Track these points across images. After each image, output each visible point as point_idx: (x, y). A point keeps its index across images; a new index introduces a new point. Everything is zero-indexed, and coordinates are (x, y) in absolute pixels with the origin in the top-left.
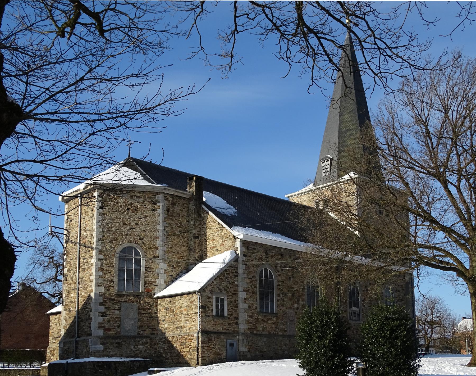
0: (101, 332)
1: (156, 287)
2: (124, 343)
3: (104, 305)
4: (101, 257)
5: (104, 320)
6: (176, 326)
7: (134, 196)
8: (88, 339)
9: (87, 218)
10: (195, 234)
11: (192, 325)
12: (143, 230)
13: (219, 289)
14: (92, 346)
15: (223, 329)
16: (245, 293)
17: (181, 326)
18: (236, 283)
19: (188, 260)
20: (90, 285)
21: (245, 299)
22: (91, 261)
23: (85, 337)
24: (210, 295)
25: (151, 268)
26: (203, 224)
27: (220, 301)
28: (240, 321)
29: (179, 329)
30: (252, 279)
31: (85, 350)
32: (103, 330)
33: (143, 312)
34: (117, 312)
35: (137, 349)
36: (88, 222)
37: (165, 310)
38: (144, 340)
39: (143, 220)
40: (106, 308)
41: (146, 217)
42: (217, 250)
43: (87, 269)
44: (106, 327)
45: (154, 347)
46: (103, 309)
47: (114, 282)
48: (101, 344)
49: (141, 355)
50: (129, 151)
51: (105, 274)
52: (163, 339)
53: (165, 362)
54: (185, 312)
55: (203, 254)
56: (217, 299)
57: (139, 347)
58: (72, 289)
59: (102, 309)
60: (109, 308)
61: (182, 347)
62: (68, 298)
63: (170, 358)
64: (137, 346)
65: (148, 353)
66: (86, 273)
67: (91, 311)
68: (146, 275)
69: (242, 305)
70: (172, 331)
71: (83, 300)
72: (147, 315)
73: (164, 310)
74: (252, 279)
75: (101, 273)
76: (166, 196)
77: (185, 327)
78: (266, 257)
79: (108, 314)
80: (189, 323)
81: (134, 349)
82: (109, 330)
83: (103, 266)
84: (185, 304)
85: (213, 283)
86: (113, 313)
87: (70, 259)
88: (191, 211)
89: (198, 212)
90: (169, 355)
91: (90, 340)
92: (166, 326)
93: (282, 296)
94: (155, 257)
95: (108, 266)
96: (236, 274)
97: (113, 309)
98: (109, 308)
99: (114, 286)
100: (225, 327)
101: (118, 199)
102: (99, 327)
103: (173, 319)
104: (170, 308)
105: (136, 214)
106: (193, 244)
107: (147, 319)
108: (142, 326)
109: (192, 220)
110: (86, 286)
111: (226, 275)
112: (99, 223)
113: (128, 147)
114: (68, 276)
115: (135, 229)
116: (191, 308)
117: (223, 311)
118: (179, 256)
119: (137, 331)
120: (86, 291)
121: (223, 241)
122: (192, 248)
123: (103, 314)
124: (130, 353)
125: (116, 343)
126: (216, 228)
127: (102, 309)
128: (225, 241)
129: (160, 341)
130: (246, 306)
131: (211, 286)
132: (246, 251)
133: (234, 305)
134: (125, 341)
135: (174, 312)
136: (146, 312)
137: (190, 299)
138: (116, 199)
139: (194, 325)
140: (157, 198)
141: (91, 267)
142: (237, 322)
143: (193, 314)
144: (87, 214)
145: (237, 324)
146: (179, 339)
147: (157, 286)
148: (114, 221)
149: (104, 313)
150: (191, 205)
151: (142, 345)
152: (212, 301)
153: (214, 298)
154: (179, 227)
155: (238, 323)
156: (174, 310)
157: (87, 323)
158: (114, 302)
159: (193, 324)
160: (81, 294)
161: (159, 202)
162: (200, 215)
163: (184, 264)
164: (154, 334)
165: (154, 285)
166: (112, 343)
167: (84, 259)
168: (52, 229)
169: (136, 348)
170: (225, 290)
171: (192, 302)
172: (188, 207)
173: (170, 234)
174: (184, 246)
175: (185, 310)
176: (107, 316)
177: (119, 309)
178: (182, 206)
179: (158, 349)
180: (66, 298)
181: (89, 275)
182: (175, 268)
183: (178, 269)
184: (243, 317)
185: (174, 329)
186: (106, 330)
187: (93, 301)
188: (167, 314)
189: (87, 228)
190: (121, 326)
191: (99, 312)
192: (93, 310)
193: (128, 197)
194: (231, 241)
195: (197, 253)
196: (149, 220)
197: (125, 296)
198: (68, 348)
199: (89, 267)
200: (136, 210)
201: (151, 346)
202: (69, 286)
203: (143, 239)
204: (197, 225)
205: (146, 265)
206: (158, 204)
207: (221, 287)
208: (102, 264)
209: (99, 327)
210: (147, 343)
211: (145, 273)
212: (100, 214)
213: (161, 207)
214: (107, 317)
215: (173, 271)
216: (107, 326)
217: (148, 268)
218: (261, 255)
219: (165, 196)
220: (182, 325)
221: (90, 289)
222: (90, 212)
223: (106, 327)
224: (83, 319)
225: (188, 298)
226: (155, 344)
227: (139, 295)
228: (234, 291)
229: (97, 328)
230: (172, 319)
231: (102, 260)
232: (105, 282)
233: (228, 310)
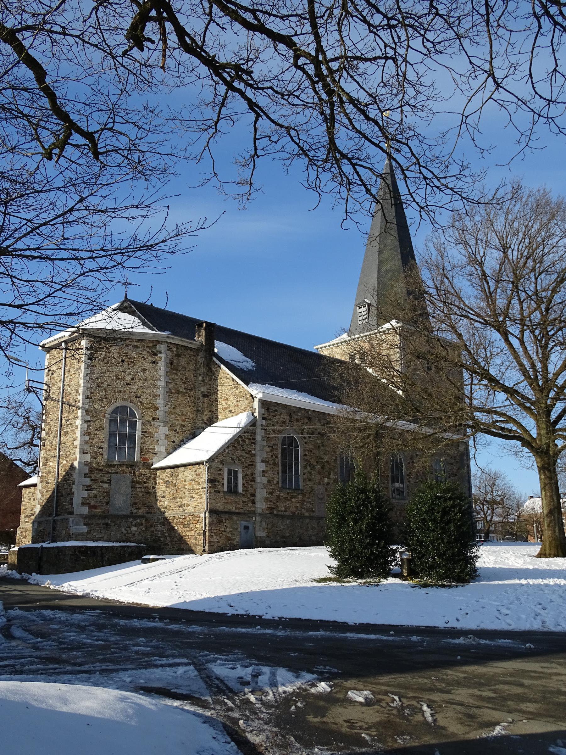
0: (85, 510)
2: (113, 524)
5: (89, 495)
6: (178, 504)
8: (67, 519)
9: (72, 371)
13: (233, 460)
18: (253, 452)
21: (263, 471)
23: (66, 516)
24: (220, 466)
27: (233, 474)
28: (257, 499)
33: (138, 485)
34: (105, 486)
38: (138, 521)
39: (140, 374)
40: (92, 480)
41: (144, 370)
47: (102, 448)
48: (85, 524)
54: (189, 487)
56: (230, 472)
59: (88, 481)
61: (185, 529)
67: (73, 484)
68: (143, 441)
69: (259, 479)
72: (143, 490)
77: (189, 505)
81: (125, 532)
82: (95, 507)
90: (169, 539)
91: (71, 519)
92: (166, 503)
93: (309, 468)
95: (97, 430)
96: (253, 442)
100: (238, 506)
102: (83, 504)
106: (201, 404)
108: (136, 504)
117: (236, 486)
120: (68, 459)
123: (89, 488)
130: (265, 480)
133: (250, 479)
140: (158, 348)
145: (253, 502)
147: (156, 454)
149: (90, 486)
151: (135, 526)
153: (226, 470)
154: (184, 383)
157: (68, 499)
159: (199, 501)
161: (161, 353)
164: (151, 513)
166: (98, 524)
167: (66, 420)
170: (240, 460)
171: (199, 475)
172: (196, 360)
175: (190, 484)
177: (109, 482)
182: (178, 433)
184: (261, 494)
186: (91, 507)
187: (77, 471)
194: (248, 401)
196: (147, 374)
199: (73, 431)
200: (132, 362)
202: (48, 453)
205: (142, 429)
206: (159, 355)
207: (234, 457)
208: (89, 426)
211: (142, 438)
213: (163, 359)
216: (93, 503)
220: (186, 502)
222: (77, 364)
225: (194, 469)
226: (151, 526)
231: (89, 421)
232: (92, 449)
233: (243, 484)
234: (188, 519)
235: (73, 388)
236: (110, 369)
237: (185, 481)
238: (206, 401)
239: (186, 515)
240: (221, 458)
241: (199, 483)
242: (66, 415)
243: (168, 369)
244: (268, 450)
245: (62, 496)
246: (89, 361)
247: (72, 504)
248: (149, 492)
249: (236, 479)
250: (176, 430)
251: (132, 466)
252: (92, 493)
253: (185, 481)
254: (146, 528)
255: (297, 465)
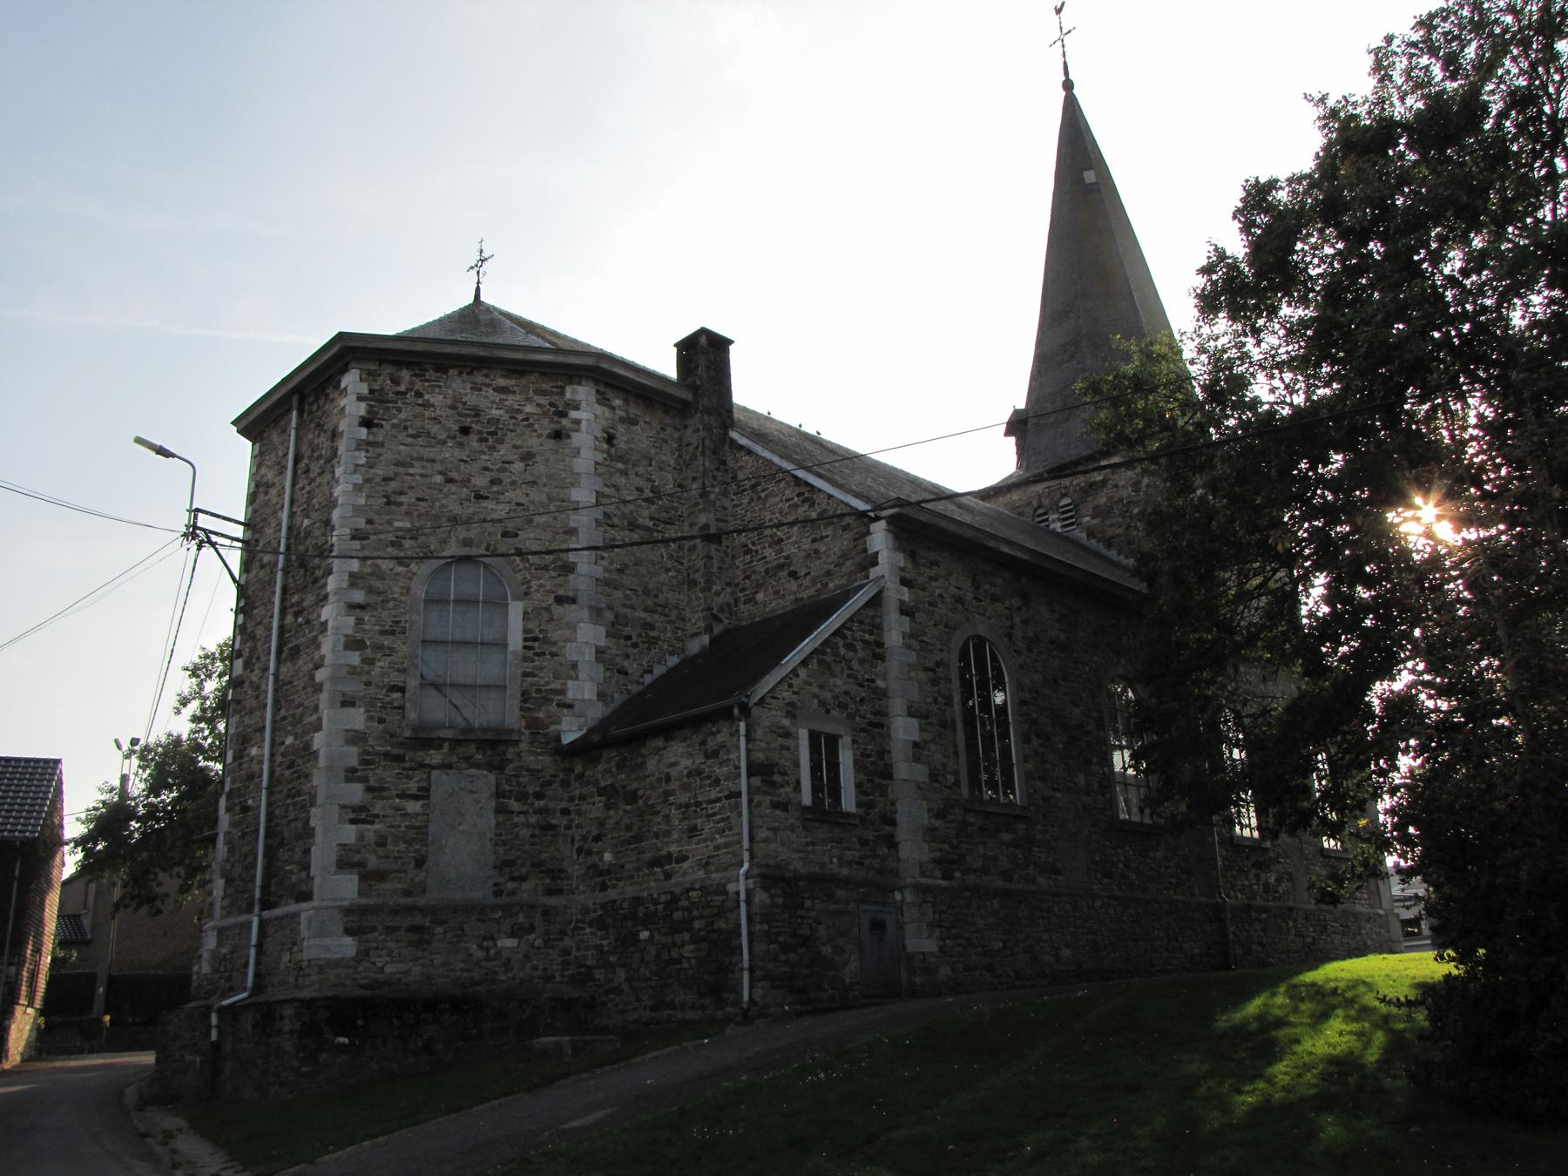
0: (348, 887)
1: (565, 711)
2: (439, 930)
3: (364, 780)
4: (359, 596)
5: (361, 837)
6: (648, 856)
7: (488, 385)
8: (296, 915)
9: (315, 469)
10: (706, 527)
11: (717, 848)
12: (518, 504)
13: (822, 703)
14: (312, 942)
15: (841, 865)
16: (915, 721)
17: (670, 855)
18: (880, 683)
19: (683, 620)
20: (312, 705)
21: (916, 745)
22: (319, 616)
23: (292, 907)
24: (786, 722)
25: (546, 641)
26: (735, 494)
27: (825, 747)
28: (903, 832)
29: (661, 866)
30: (934, 671)
31: (286, 957)
32: (356, 878)
33: (514, 805)
34: (413, 807)
35: (492, 951)
36: (318, 480)
37: (604, 798)
38: (521, 918)
39: (518, 466)
40: (369, 789)
41: (528, 457)
42: (794, 575)
43: (307, 647)
44: (370, 865)
45: (562, 944)
46: (360, 794)
47: (402, 690)
48: (349, 932)
49: (510, 975)
50: (478, 283)
51: (370, 662)
52: (595, 911)
53: (605, 1004)
54: (684, 798)
55: (736, 601)
56: (814, 737)
57: (499, 944)
58: (255, 731)
59: (355, 793)
60: (384, 789)
61: (678, 938)
62: (240, 765)
63: (625, 987)
64: (493, 939)
65: (535, 968)
66: (300, 662)
67: (313, 803)
68: (528, 667)
69: (904, 769)
70: (632, 877)
71: (286, 764)
72: (533, 819)
73: (597, 799)
74: (935, 673)
75: (355, 658)
76: (603, 389)
77: (685, 858)
78: (976, 599)
79: (377, 816)
80: (705, 840)
81: (480, 954)
82: (381, 876)
83: (365, 631)
84: (686, 763)
85: (797, 675)
86: (397, 809)
87: (253, 623)
88: (691, 448)
89: (715, 453)
90: (621, 973)
91: (303, 916)
92: (608, 857)
93: (1036, 742)
94: (560, 600)
95: (383, 633)
96: (877, 652)
97: (399, 796)
98: (384, 789)
99: (402, 708)
100: (849, 855)
101: (427, 397)
102: (344, 864)
103: (635, 828)
104: (624, 787)
105: (493, 448)
106: (700, 564)
107: (533, 836)
108: (511, 863)
109: (694, 479)
110: (300, 710)
111: (843, 651)
112: (357, 476)
113: (474, 272)
114: (247, 684)
115: (487, 498)
116: (709, 777)
117: (836, 792)
118: (650, 603)
119: (491, 882)
120: (299, 730)
121: (814, 540)
122: (697, 576)
123: (360, 815)
124: (462, 970)
125: (411, 929)
126: (787, 500)
127: (355, 793)
128: (822, 538)
129: (583, 921)
130: (921, 773)
131: (790, 686)
132: (910, 566)
133: (876, 771)
134: (445, 922)
135: (641, 802)
136: (525, 808)
137: (703, 743)
138: (419, 394)
139: (726, 845)
140: (568, 395)
141: (320, 636)
142: (891, 836)
143: (719, 800)
144: (316, 455)
145: (892, 843)
146: (660, 907)
147: (570, 706)
148: (411, 471)
149: (362, 808)
150: (690, 431)
151: (512, 935)
152: (797, 747)
153: (803, 735)
154: (648, 500)
155: (898, 839)
156: (640, 793)
157: (298, 852)
158: (404, 769)
159: (720, 840)
160: (283, 743)
161: (577, 408)
162: (724, 463)
163: (669, 634)
164: (559, 892)
165: (559, 705)
166: (391, 930)
167: (297, 615)
168: (196, 517)
169: (487, 950)
170: (843, 706)
171: (714, 754)
172: (680, 439)
173: (616, 521)
174: (668, 570)
175: (686, 787)
176: (372, 823)
177: (423, 794)
178: (658, 433)
179: (574, 953)
180: (236, 763)
181: (311, 666)
182: (635, 645)
183: (649, 649)
184: (911, 814)
185: (638, 869)
186: (369, 877)
187: (322, 762)
188: (612, 813)
189: (314, 501)
190: (429, 864)
191: (342, 807)
192: (320, 800)
193: (464, 389)
194: (848, 535)
195: (718, 594)
196: (539, 469)
197: (446, 745)
198: (232, 953)
199: (314, 640)
200: (494, 434)
201: (546, 942)
202: (247, 721)
203: (516, 535)
204: (712, 496)
205: (526, 631)
206: (573, 414)
207: (827, 695)
208: (360, 621)
209: (344, 864)
210: (532, 929)
211: (525, 659)
212: (358, 444)
213: (584, 425)
214: (377, 826)
215: (627, 656)
216: (373, 862)
217: (535, 639)
218: (960, 589)
219: (598, 391)
220: (674, 848)
221: (314, 717)
222: (327, 444)
223: (370, 865)
224: (286, 834)
225: (696, 739)
226: (563, 933)
227: (500, 742)
228: (876, 714)
229: (333, 869)
230: (629, 828)
231: (361, 607)
232: (372, 690)
233: (858, 786)
234: (684, 903)
235: (314, 515)
236: (428, 453)
237: (668, 778)
238: (714, 554)
239: (678, 890)
240: (787, 695)
241: (717, 782)
242: (295, 599)
243: (600, 457)
244: (923, 676)
245: (281, 845)
246: (364, 431)
247: (307, 867)
248: (553, 827)
249: (834, 767)
250: (628, 638)
251: (494, 743)
252: (371, 830)
253: (668, 778)
254: (547, 943)
255: (1005, 735)
